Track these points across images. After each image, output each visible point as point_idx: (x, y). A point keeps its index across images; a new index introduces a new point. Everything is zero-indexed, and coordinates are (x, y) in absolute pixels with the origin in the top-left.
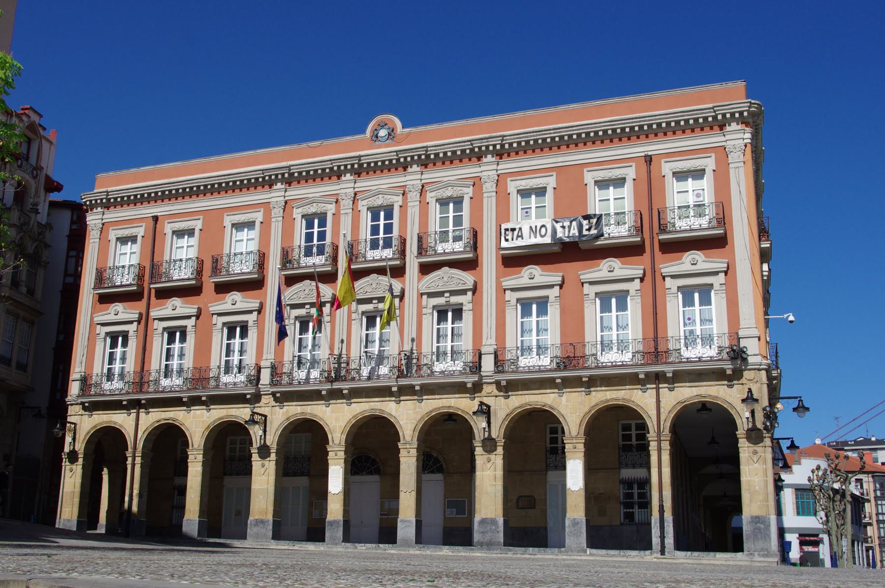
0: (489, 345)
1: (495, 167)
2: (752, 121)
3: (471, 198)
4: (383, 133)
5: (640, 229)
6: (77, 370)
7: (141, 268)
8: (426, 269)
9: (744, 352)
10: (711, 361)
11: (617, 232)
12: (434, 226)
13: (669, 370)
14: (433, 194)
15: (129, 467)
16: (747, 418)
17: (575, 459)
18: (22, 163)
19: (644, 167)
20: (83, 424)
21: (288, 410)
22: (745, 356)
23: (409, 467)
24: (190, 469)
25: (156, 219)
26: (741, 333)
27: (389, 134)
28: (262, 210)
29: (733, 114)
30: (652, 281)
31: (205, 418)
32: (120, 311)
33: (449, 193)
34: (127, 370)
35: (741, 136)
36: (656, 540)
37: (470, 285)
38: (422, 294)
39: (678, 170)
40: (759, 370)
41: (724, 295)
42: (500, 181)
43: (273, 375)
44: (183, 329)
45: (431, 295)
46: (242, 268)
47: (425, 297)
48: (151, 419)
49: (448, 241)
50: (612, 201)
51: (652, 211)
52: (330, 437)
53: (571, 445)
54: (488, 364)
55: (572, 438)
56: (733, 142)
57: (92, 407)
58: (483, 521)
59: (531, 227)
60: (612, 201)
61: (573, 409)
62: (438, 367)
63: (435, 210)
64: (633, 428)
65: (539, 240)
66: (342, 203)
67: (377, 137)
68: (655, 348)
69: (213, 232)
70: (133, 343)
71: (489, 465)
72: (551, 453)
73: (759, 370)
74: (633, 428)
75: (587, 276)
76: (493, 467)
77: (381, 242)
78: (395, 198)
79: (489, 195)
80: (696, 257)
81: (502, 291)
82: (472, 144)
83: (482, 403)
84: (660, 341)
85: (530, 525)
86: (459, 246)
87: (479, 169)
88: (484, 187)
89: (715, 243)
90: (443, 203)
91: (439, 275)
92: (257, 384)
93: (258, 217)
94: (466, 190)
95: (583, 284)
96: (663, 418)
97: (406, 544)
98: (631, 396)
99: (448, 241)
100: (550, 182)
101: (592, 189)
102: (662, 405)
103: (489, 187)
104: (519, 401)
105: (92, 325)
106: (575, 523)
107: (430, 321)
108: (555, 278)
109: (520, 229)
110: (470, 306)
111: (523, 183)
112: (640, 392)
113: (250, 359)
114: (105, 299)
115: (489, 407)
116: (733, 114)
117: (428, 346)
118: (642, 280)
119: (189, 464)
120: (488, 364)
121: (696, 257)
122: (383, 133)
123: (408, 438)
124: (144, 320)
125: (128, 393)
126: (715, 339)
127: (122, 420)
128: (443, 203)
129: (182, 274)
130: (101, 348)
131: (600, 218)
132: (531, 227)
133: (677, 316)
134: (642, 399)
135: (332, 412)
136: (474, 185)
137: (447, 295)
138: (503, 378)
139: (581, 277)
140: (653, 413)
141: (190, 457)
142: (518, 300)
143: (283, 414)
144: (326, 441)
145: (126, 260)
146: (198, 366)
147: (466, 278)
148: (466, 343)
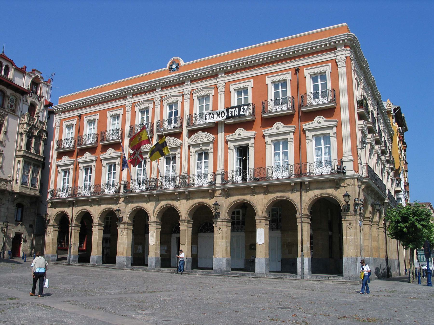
2: (351, 44)
3: (213, 96)
4: (174, 66)
5: (293, 108)
6: (51, 186)
7: (75, 139)
8: (191, 133)
9: (344, 169)
12: (196, 110)
14: (196, 95)
15: (70, 231)
17: (260, 228)
18: (32, 95)
20: (52, 213)
22: (344, 171)
26: (344, 159)
27: (177, 67)
28: (123, 108)
30: (301, 133)
32: (66, 159)
34: (91, 184)
35: (344, 52)
37: (211, 140)
38: (57, 166)
39: (312, 73)
40: (354, 179)
42: (133, 105)
43: (222, 179)
44: (285, 141)
45: (61, 166)
46: (112, 137)
47: (191, 147)
48: (78, 210)
49: (318, 98)
51: (102, 134)
54: (122, 190)
55: (182, 221)
57: (54, 205)
63: (197, 103)
66: (156, 102)
69: (103, 122)
70: (71, 174)
71: (220, 231)
73: (354, 179)
77: (281, 101)
78: (179, 98)
80: (279, 125)
84: (303, 166)
85: (139, 259)
86: (325, 100)
87: (124, 102)
89: (329, 112)
90: (238, 92)
91: (197, 136)
92: (119, 193)
93: (121, 112)
94: (210, 92)
97: (123, 267)
99: (279, 104)
100: (250, 84)
101: (109, 119)
102: (303, 199)
103: (221, 89)
104: (233, 199)
105: (227, 142)
107: (194, 158)
110: (212, 151)
111: (237, 86)
113: (117, 180)
114: (60, 155)
116: (339, 41)
117: (194, 171)
118: (294, 132)
120: (122, 190)
122: (174, 66)
124: (77, 164)
125: (67, 198)
126: (324, 163)
127: (68, 210)
128: (201, 98)
129: (89, 141)
130: (61, 176)
133: (312, 153)
134: (294, 197)
138: (226, 186)
139: (264, 133)
142: (84, 167)
144: (255, 215)
145: (68, 135)
146: (259, 166)
147: (210, 137)
148: (210, 170)
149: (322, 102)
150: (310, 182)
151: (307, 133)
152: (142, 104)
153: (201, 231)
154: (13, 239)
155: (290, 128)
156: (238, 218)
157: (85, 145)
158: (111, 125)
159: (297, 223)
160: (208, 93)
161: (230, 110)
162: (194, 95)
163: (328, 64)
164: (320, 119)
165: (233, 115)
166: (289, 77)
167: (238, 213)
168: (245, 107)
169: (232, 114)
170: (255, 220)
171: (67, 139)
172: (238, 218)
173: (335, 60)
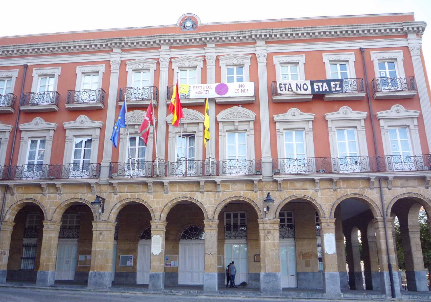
0: (107, 160)
1: (119, 55)
10: (403, 171)
11: (350, 90)
13: (335, 177)
19: (359, 55)
21: (120, 196)
23: (212, 237)
24: (44, 235)
25: (26, 66)
26: (102, 164)
29: (413, 28)
31: (57, 200)
33: (235, 61)
36: (387, 288)
39: (85, 71)
41: (417, 132)
50: (141, 80)
52: (152, 215)
53: (325, 224)
54: (267, 170)
56: (209, 54)
58: (268, 275)
59: (297, 85)
60: (141, 80)
61: (325, 201)
64: (286, 215)
65: (303, 92)
67: (184, 26)
68: (324, 163)
71: (269, 237)
72: (227, 230)
74: (286, 215)
75: (330, 116)
76: (272, 238)
79: (262, 64)
81: (273, 123)
82: (251, 33)
83: (97, 196)
85: (411, 287)
88: (112, 67)
91: (231, 111)
94: (152, 65)
95: (65, 130)
96: (385, 207)
98: (364, 193)
103: (164, 65)
106: (332, 276)
108: (311, 116)
109: (290, 84)
112: (370, 191)
115: (103, 200)
119: (44, 232)
120: (267, 170)
121: (348, 111)
122: (188, 24)
123: (327, 215)
131: (341, 81)
132: (297, 85)
134: (372, 195)
135: (154, 198)
136: (251, 58)
137: (185, 125)
140: (379, 203)
141: (152, 227)
143: (117, 198)
144: (150, 218)
147: (250, 114)
149: (399, 90)
150: (284, 180)
151: (23, 133)
152: (139, 63)
153: (184, 237)
154: (362, 243)
155: (52, 125)
156: (228, 223)
157: (33, 104)
158: (39, 87)
159: (92, 231)
160: (242, 62)
161: (315, 84)
162: (174, 64)
163: (399, 51)
164: (295, 111)
165: (321, 90)
166: (352, 58)
167: (228, 216)
168: (336, 83)
169: (319, 88)
170: (92, 225)
171: (5, 96)
172: (228, 223)
173: (408, 47)
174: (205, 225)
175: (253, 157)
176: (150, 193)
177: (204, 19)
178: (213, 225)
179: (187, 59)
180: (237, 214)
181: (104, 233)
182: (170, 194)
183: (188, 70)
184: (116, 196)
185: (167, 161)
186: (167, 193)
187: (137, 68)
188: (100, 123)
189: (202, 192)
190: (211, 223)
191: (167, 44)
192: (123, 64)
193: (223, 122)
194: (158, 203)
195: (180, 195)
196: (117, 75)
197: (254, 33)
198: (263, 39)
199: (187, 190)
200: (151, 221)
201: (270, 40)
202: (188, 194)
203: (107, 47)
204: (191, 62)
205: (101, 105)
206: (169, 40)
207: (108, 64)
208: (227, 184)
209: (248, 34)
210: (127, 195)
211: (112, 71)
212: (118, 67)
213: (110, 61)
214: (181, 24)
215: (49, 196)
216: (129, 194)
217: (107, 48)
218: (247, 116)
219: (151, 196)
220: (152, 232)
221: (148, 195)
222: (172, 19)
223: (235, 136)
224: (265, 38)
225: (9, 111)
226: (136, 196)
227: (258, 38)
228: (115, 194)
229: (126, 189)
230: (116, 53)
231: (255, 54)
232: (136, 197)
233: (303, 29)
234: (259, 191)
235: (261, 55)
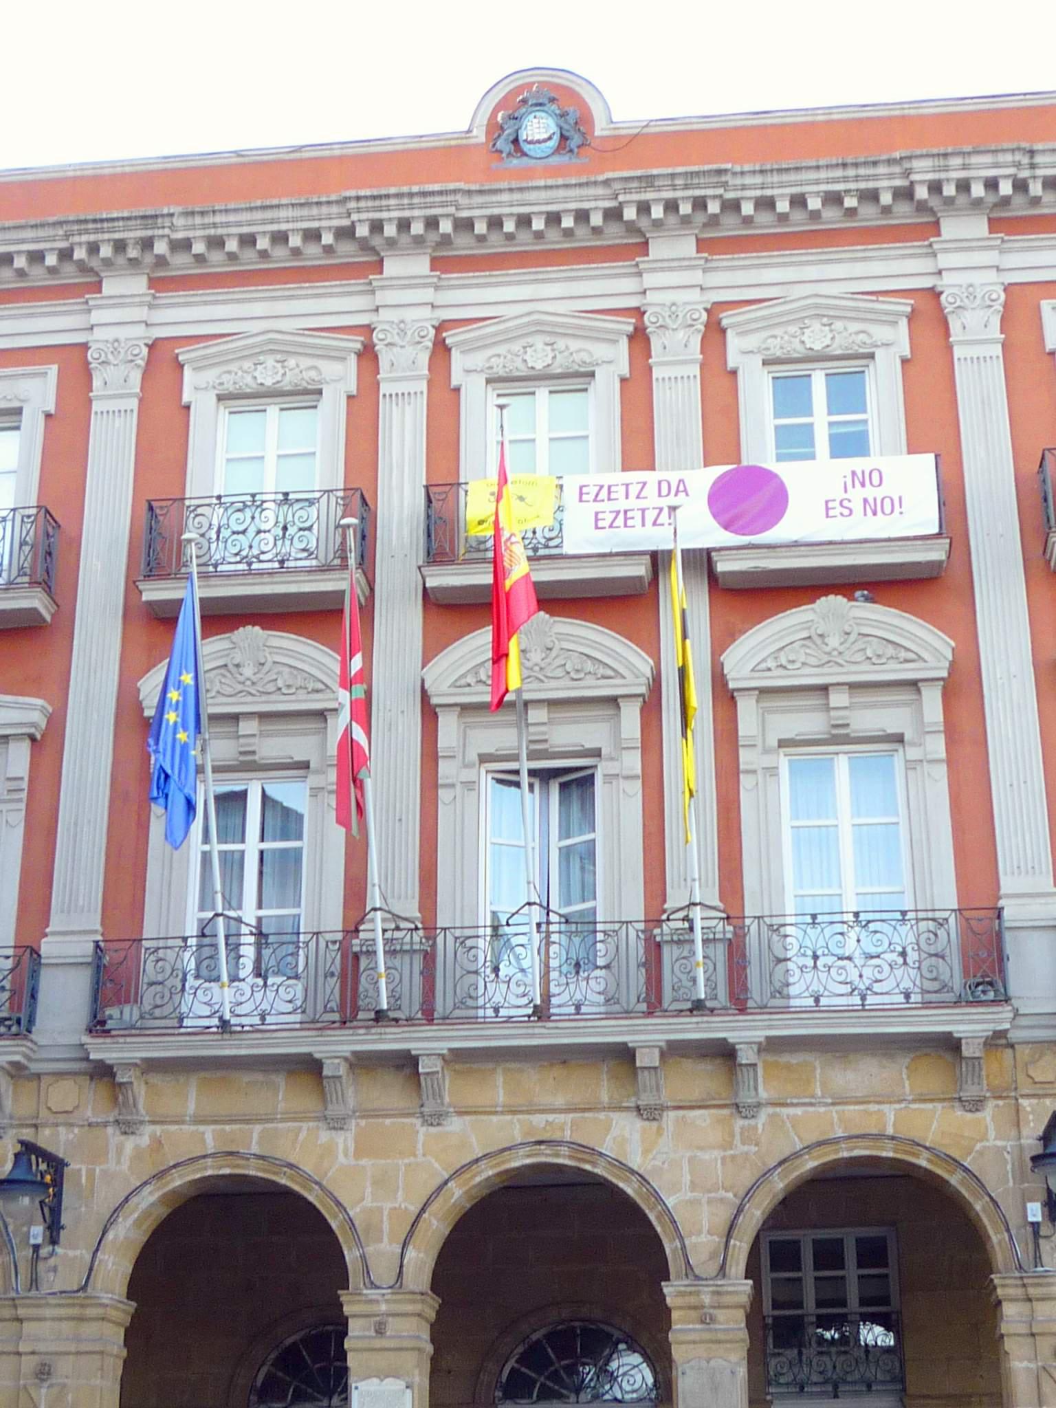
16: (36, 1248)
21: (157, 1143)
26: (48, 948)
62: (200, 1005)
67: (516, 141)
88: (97, 383)
94: (330, 369)
103: (405, 368)
115: (57, 1165)
122: (539, 128)
135: (358, 1154)
136: (911, 318)
137: (246, 727)
147: (922, 642)
152: (255, 355)
162: (734, 343)
170: (668, 1311)
174: (675, 1315)
175: (946, 896)
176: (338, 1124)
177: (629, 99)
178: (721, 1315)
179: (540, 328)
180: (796, 1244)
181: (64, 1367)
182: (455, 1125)
183: (542, 393)
184: (130, 1144)
185: (430, 929)
186: (435, 1119)
187: (248, 383)
188: (32, 708)
189: (648, 1113)
190: (707, 1299)
191: (686, 221)
192: (163, 362)
193: (764, 692)
194: (382, 1182)
195: (513, 1129)
196: (995, 375)
197: (923, 172)
198: (978, 203)
199: (560, 1101)
200: (344, 1296)
201: (1020, 208)
202: (563, 1125)
203: (69, 268)
204: (561, 343)
205: (35, 601)
206: (432, 223)
207: (76, 365)
208: (794, 1059)
209: (891, 176)
210: (197, 1138)
211: (96, 406)
212: (136, 377)
213: (85, 347)
214: (494, 129)
215: (771, 1116)
216: (209, 1131)
217: (70, 275)
218: (903, 654)
219: (344, 1141)
220: (352, 1361)
221: (325, 1136)
222: (448, 108)
223: (831, 770)
224: (991, 199)
225: (34, 611)
226: (254, 1139)
227: (950, 201)
228: (127, 1128)
229: (190, 1097)
230: (120, 301)
231: (935, 294)
232: (255, 1149)
233: (179, 222)
234: (991, 1105)
235: (972, 296)
